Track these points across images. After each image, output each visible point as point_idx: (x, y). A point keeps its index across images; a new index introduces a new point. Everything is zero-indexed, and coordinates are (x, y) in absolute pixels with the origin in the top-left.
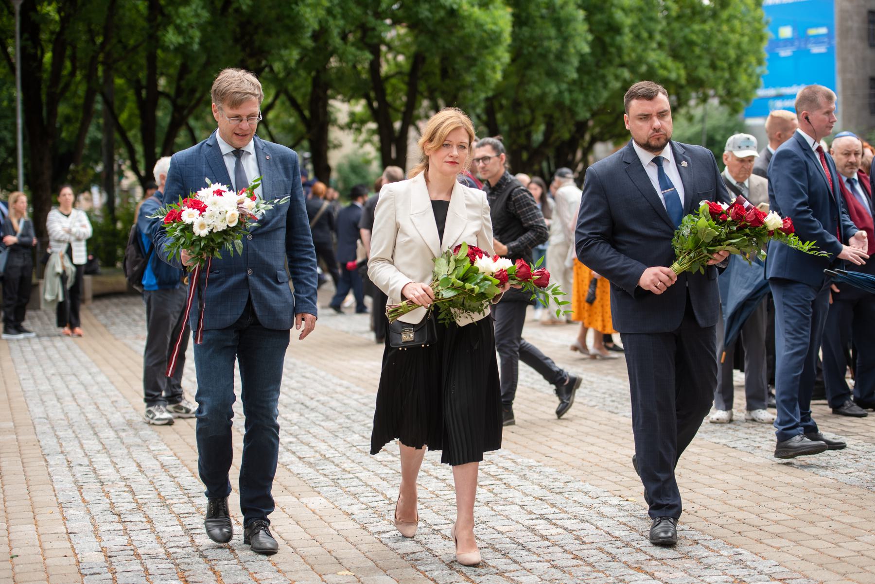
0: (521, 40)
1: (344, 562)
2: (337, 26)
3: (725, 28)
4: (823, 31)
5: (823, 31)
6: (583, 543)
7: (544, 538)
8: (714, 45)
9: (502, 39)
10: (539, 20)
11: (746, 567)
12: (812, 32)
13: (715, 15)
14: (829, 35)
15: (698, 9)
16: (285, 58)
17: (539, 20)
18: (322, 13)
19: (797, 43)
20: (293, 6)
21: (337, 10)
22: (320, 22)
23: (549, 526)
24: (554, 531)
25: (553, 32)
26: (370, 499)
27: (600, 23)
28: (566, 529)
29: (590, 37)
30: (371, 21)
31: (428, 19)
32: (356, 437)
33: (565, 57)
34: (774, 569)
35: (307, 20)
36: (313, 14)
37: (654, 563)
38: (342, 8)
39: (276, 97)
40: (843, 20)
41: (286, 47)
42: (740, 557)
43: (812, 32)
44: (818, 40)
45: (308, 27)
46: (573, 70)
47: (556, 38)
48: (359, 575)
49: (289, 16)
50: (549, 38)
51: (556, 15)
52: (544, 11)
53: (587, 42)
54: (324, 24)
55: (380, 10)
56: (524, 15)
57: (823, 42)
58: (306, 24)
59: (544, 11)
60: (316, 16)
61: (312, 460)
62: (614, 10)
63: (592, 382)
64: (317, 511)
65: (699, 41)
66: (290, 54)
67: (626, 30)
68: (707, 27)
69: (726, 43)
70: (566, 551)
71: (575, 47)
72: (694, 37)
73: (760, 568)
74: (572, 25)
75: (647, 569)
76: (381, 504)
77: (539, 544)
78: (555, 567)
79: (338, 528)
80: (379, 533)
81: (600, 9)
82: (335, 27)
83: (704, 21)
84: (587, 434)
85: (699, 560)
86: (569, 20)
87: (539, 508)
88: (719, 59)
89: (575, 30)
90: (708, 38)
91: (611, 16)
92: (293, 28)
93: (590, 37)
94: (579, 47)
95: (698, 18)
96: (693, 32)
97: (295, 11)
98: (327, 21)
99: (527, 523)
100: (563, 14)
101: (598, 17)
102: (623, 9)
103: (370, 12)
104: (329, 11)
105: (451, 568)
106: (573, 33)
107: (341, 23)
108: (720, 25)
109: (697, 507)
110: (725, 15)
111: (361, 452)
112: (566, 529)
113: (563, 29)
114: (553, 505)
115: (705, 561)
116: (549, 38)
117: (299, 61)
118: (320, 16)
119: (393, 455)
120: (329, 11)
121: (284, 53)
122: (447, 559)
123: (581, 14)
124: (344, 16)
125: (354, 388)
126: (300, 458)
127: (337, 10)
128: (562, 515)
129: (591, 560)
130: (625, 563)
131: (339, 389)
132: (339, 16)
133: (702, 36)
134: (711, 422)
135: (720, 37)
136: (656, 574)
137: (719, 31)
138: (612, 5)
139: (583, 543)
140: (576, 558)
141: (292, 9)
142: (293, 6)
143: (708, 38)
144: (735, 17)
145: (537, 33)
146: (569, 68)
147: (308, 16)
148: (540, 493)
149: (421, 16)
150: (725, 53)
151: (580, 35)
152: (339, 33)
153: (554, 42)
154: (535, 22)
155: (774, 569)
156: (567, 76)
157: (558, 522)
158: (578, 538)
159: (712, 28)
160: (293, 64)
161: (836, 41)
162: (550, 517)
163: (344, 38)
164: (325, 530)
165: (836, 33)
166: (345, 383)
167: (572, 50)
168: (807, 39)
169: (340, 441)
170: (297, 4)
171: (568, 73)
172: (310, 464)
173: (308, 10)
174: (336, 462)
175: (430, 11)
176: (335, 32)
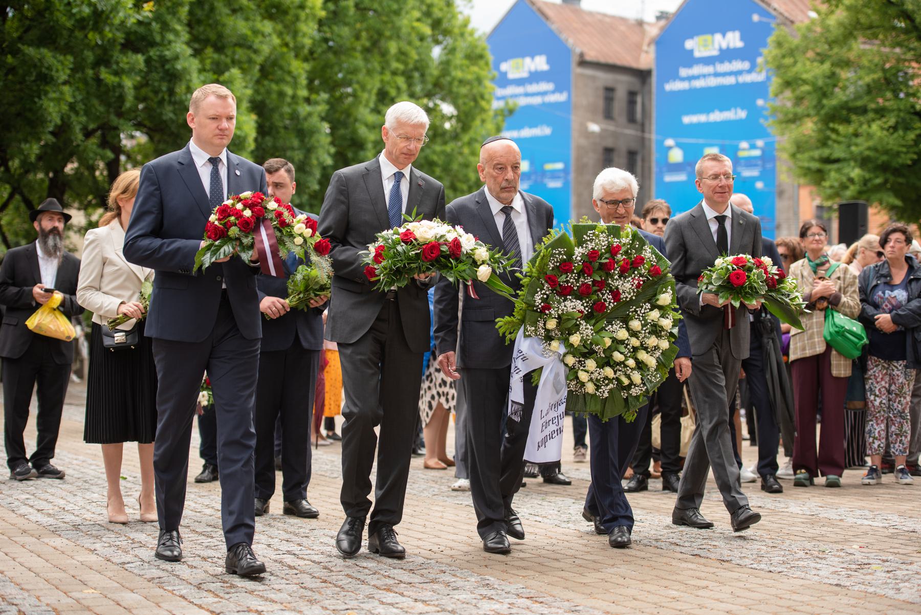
0: (264, 149)
1: (90, 584)
2: (80, 123)
3: (466, 150)
4: (559, 166)
5: (559, 166)
6: (332, 571)
7: (290, 567)
8: (455, 166)
9: (247, 145)
10: (282, 131)
11: (494, 588)
12: (549, 167)
13: (456, 137)
14: (565, 171)
15: (440, 131)
16: (26, 153)
17: (282, 131)
18: (65, 108)
19: (533, 177)
20: (36, 100)
21: (80, 107)
22: (62, 119)
23: (296, 559)
24: (301, 562)
25: (296, 143)
26: (113, 540)
27: (343, 138)
28: (313, 562)
29: (333, 150)
30: (114, 120)
31: (172, 121)
32: (96, 495)
33: (308, 169)
34: (521, 591)
35: (50, 114)
36: (57, 109)
37: (402, 585)
38: (85, 105)
39: (11, 196)
40: (578, 159)
41: (26, 141)
42: (487, 582)
43: (549, 167)
44: (554, 175)
45: (50, 122)
46: (315, 182)
47: (299, 149)
48: (105, 593)
49: (30, 110)
50: (293, 149)
51: (299, 126)
52: (287, 122)
53: (329, 154)
54: (66, 120)
55: (123, 109)
56: (267, 124)
57: (559, 177)
58: (49, 119)
59: (287, 122)
60: (59, 111)
61: (51, 512)
62: (357, 125)
63: (333, 461)
64: (59, 548)
65: (440, 162)
66: (31, 148)
67: (370, 146)
68: (448, 148)
69: (466, 165)
70: (314, 577)
71: (318, 159)
72: (435, 158)
73: (508, 589)
74: (316, 136)
75: (396, 590)
76: (125, 543)
77: (287, 572)
78: (305, 588)
79: (80, 559)
80: (124, 563)
81: (345, 125)
82: (78, 122)
83: (445, 143)
84: (330, 497)
85: (448, 584)
86: (313, 132)
87: (285, 547)
88: (460, 181)
89: (318, 141)
90: (449, 157)
91: (355, 132)
92: (33, 122)
93: (333, 150)
94: (321, 159)
95: (439, 140)
96: (434, 152)
97: (38, 105)
98: (69, 117)
99: (274, 557)
100: (306, 125)
101: (342, 131)
102: (367, 125)
103: (112, 110)
104: (72, 107)
105: (199, 588)
106: (316, 144)
107: (83, 119)
108: (461, 147)
109: (442, 548)
110: (466, 138)
111: (100, 506)
112: (313, 562)
113: (307, 140)
114: (299, 545)
115: (452, 585)
116: (293, 149)
117: (40, 158)
118: (64, 111)
119: (134, 509)
120: (72, 107)
121: (25, 146)
122: (195, 582)
123: (326, 127)
124: (87, 113)
125: (90, 461)
126: (38, 510)
127: (80, 107)
128: (309, 552)
129: (340, 583)
130: (374, 586)
131: (75, 462)
132: (82, 112)
133: (442, 157)
134: (453, 490)
135: (461, 159)
136: (405, 593)
137: (461, 154)
138: (356, 120)
139: (332, 571)
140: (325, 582)
141: (35, 103)
142: (36, 100)
143: (449, 157)
144: (476, 140)
145: (280, 143)
146: (310, 179)
147: (51, 110)
148: (286, 536)
149: (164, 118)
150: (466, 176)
151: (323, 147)
152: (81, 129)
153: (296, 152)
154: (278, 132)
155: (521, 591)
156: (309, 188)
157: (305, 557)
158: (325, 568)
159: (453, 150)
160: (33, 158)
161: (572, 176)
162: (297, 553)
163: (88, 134)
164: (69, 561)
165: (572, 168)
166: (81, 458)
167: (314, 162)
168: (544, 173)
169: (78, 498)
170: (40, 98)
171: (310, 185)
172: (49, 515)
173: (52, 104)
174: (76, 513)
175: (174, 112)
176: (77, 129)
